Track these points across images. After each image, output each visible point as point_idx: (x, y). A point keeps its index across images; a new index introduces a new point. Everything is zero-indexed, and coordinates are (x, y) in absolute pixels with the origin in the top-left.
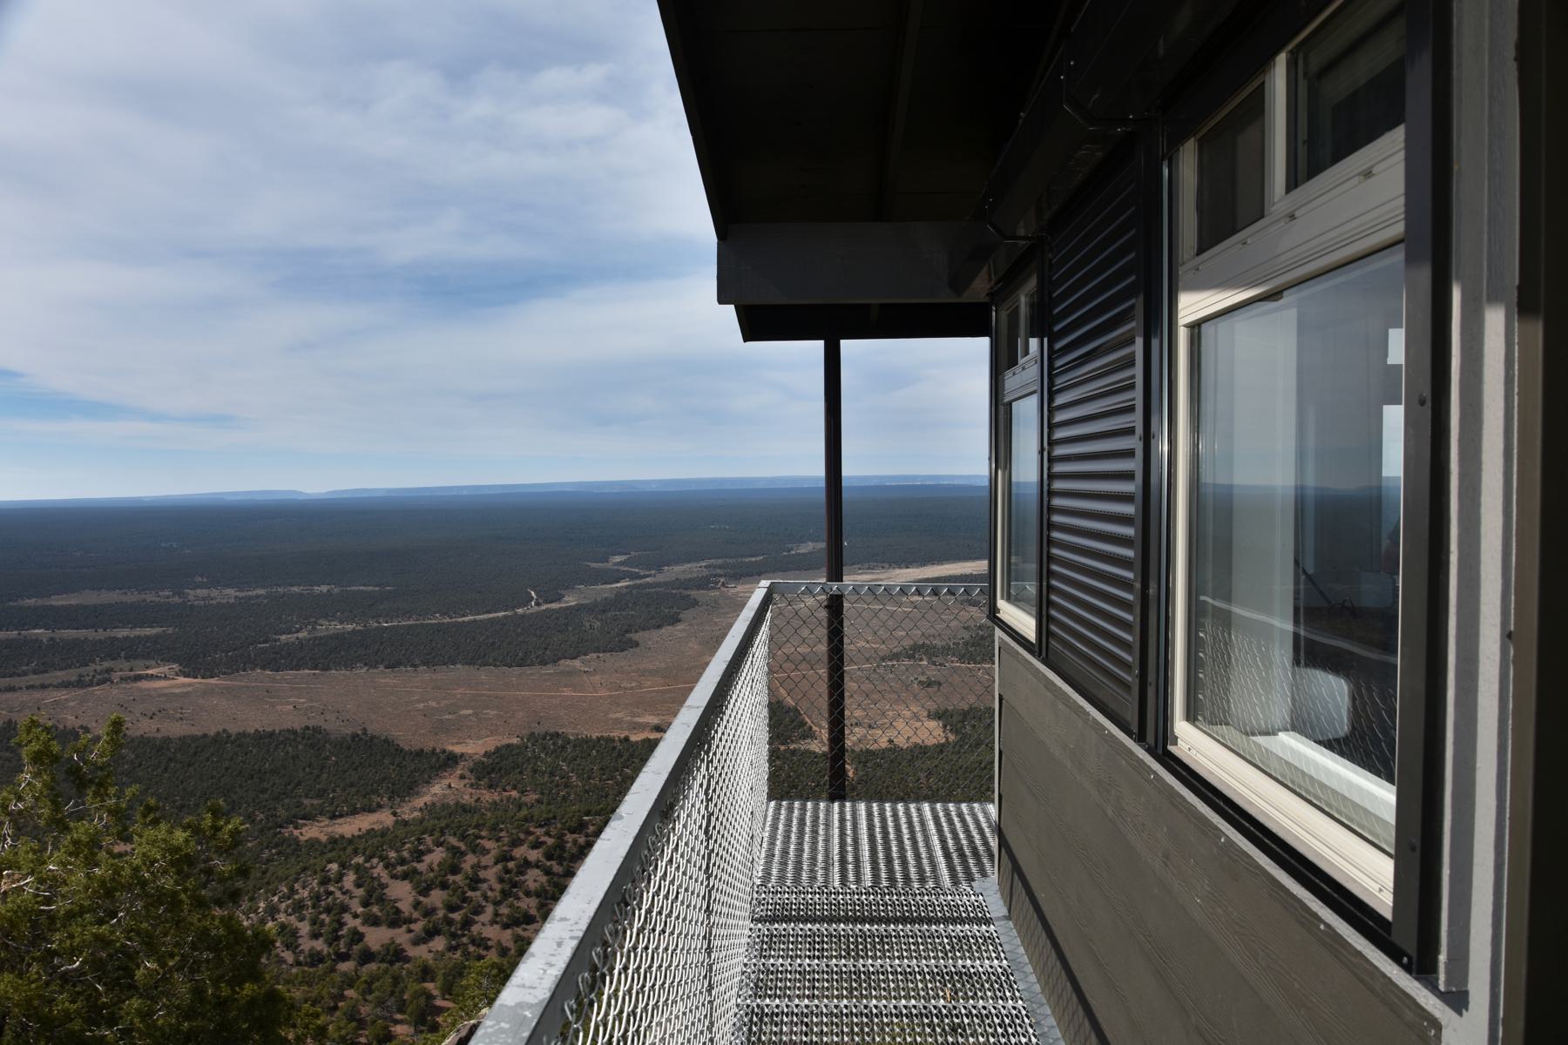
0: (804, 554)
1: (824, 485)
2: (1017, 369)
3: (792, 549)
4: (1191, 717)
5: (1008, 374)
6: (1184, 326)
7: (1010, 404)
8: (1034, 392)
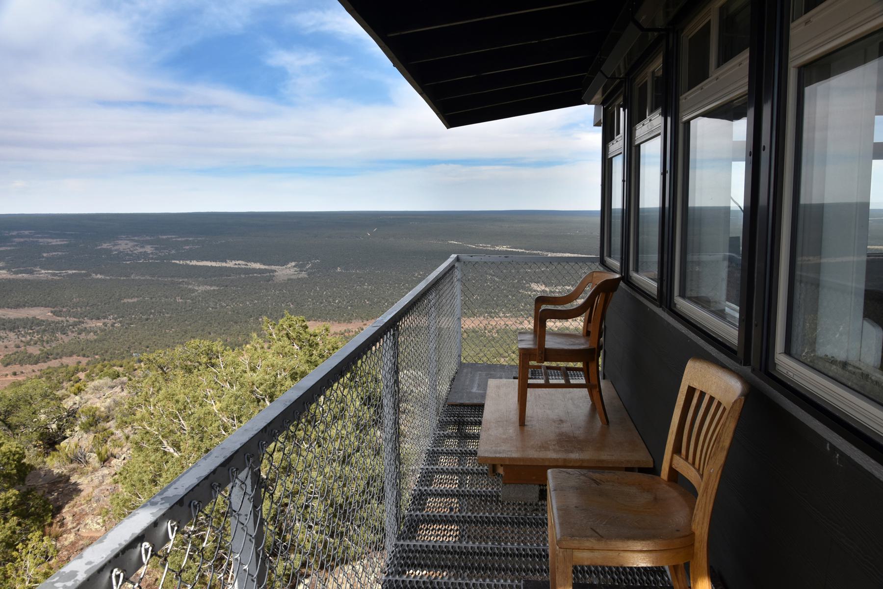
1: (745, 139)
2: (614, 142)
4: (788, 352)
5: (610, 144)
6: (793, 67)
7: (639, 146)
8: (621, 153)
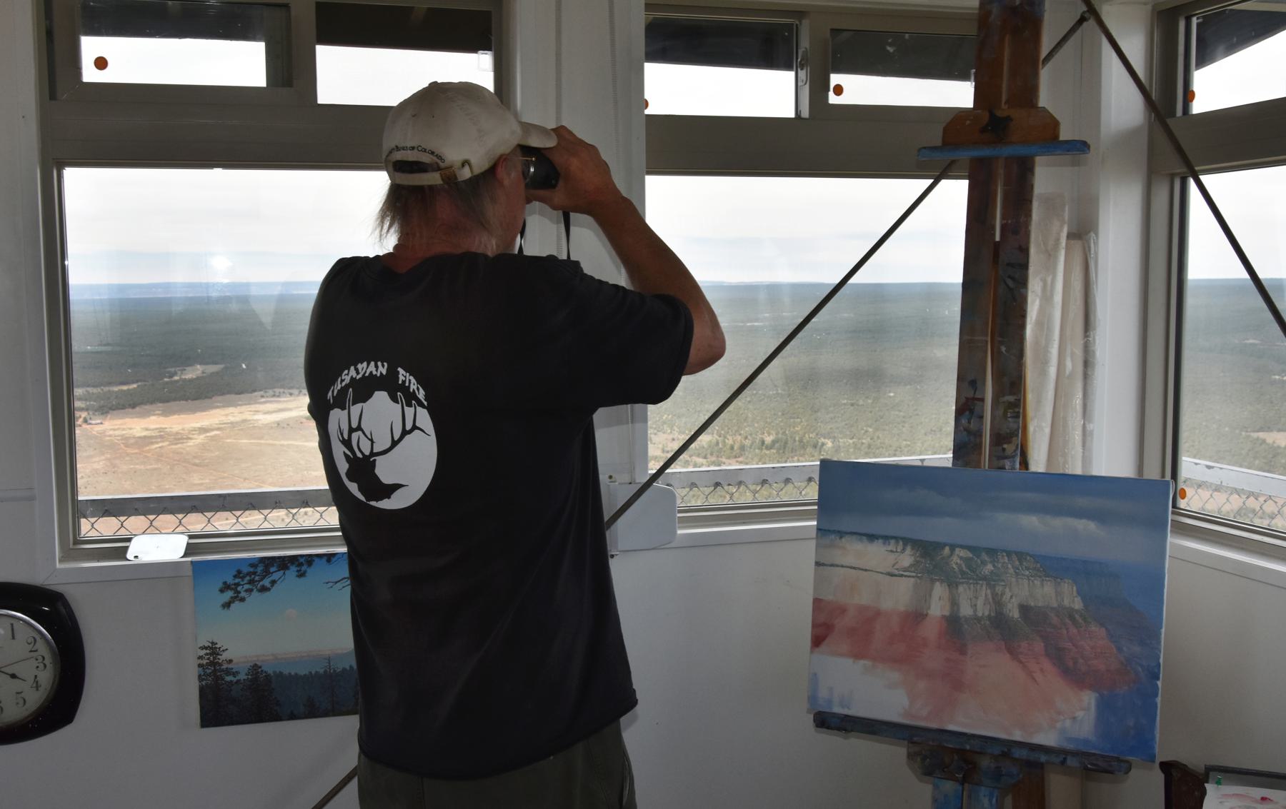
0: (191, 380)
3: (175, 374)
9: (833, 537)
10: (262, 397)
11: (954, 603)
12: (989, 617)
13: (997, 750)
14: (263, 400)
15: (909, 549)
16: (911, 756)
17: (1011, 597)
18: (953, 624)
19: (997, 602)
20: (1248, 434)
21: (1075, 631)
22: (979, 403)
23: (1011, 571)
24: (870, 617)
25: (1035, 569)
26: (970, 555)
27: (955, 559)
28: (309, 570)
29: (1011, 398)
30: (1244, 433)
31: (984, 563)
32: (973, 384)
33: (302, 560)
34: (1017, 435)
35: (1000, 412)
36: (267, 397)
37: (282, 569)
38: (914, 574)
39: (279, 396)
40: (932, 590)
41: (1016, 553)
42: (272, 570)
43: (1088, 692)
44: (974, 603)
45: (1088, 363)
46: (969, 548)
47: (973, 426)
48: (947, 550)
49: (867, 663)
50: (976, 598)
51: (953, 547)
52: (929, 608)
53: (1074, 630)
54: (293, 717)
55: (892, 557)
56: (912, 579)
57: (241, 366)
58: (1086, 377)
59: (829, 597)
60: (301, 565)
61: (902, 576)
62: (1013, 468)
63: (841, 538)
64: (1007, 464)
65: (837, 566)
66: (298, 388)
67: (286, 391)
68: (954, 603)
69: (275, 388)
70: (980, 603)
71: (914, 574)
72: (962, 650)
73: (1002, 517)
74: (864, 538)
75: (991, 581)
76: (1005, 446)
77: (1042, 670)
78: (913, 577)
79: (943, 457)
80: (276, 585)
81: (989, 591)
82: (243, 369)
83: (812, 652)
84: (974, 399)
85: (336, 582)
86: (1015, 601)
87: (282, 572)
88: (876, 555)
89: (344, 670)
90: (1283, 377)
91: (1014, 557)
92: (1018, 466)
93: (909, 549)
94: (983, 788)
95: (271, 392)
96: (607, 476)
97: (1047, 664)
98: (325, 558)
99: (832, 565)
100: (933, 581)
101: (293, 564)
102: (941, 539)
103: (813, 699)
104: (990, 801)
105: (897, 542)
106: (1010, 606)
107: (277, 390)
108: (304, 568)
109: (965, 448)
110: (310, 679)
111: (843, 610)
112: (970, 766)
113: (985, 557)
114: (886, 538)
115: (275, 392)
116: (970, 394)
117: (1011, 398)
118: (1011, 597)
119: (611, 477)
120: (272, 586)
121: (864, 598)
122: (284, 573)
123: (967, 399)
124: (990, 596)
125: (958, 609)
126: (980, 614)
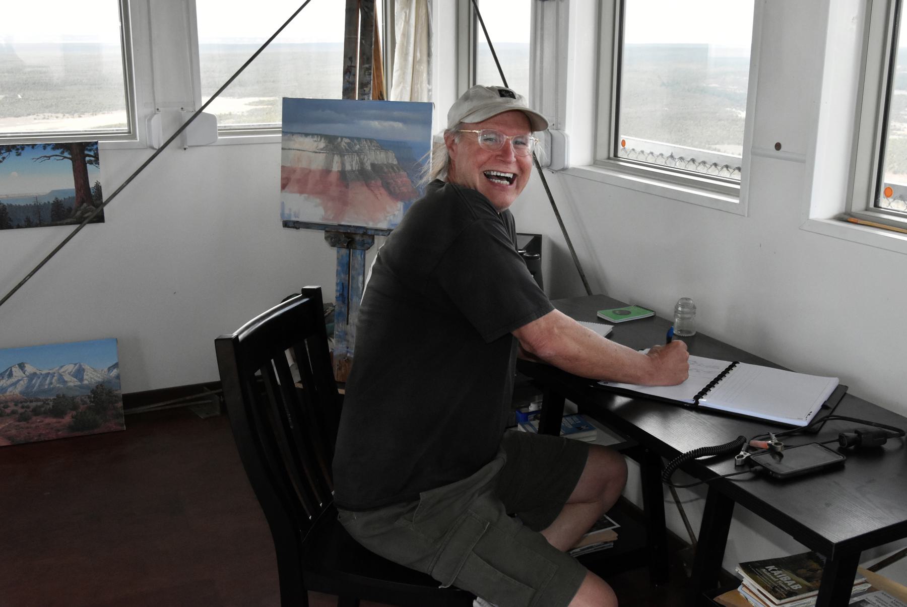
9: (289, 135)
10: (35, 119)
11: (343, 164)
12: (358, 170)
13: (361, 232)
14: (36, 121)
15: (323, 140)
16: (326, 238)
17: (367, 161)
18: (343, 174)
19: (362, 163)
20: (710, 146)
21: (394, 174)
22: (353, 68)
23: (367, 148)
24: (307, 173)
25: (377, 146)
26: (349, 141)
27: (343, 143)
28: (22, 152)
29: (367, 66)
30: (707, 146)
31: (355, 145)
32: (351, 59)
33: (19, 147)
34: (370, 84)
35: (363, 72)
36: (39, 119)
37: (8, 151)
38: (325, 152)
39: (48, 119)
40: (333, 158)
41: (369, 139)
42: (2, 152)
43: (400, 202)
44: (351, 164)
45: (429, 55)
46: (349, 138)
47: (351, 80)
48: (339, 139)
49: (306, 195)
50: (353, 161)
51: (342, 138)
52: (332, 167)
53: (393, 174)
54: (19, 227)
55: (316, 144)
56: (325, 154)
57: (17, 96)
58: (429, 62)
59: (288, 165)
60: (18, 149)
61: (320, 153)
62: (369, 99)
63: (293, 135)
64: (366, 97)
65: (291, 149)
66: (63, 113)
67: (53, 115)
68: (343, 164)
69: (44, 113)
70: (354, 163)
71: (325, 152)
72: (347, 186)
73: (363, 123)
74: (303, 135)
75: (359, 153)
76: (365, 89)
77: (381, 194)
78: (323, 153)
79: (337, 94)
80: (5, 160)
81: (358, 158)
82: (19, 99)
83: (281, 192)
84: (351, 66)
85: (38, 159)
86: (369, 162)
87: (8, 153)
88: (308, 143)
89: (45, 203)
90: (732, 109)
91: (368, 141)
92: (371, 98)
93: (323, 140)
94: (358, 251)
95: (41, 116)
96: (180, 108)
97: (383, 190)
98: (31, 147)
99: (289, 149)
100: (334, 154)
101: (13, 149)
102: (336, 134)
103: (282, 215)
104: (361, 256)
105: (318, 137)
106: (367, 164)
107: (46, 115)
108: (20, 151)
109: (348, 90)
110: (26, 208)
111: (294, 171)
112: (350, 240)
113: (356, 141)
114: (313, 135)
115: (45, 116)
116: (349, 64)
117: (367, 66)
118: (367, 161)
119: (182, 109)
120: (3, 160)
121: (304, 164)
122: (9, 154)
123: (348, 66)
124: (358, 160)
125: (345, 167)
126: (354, 169)
